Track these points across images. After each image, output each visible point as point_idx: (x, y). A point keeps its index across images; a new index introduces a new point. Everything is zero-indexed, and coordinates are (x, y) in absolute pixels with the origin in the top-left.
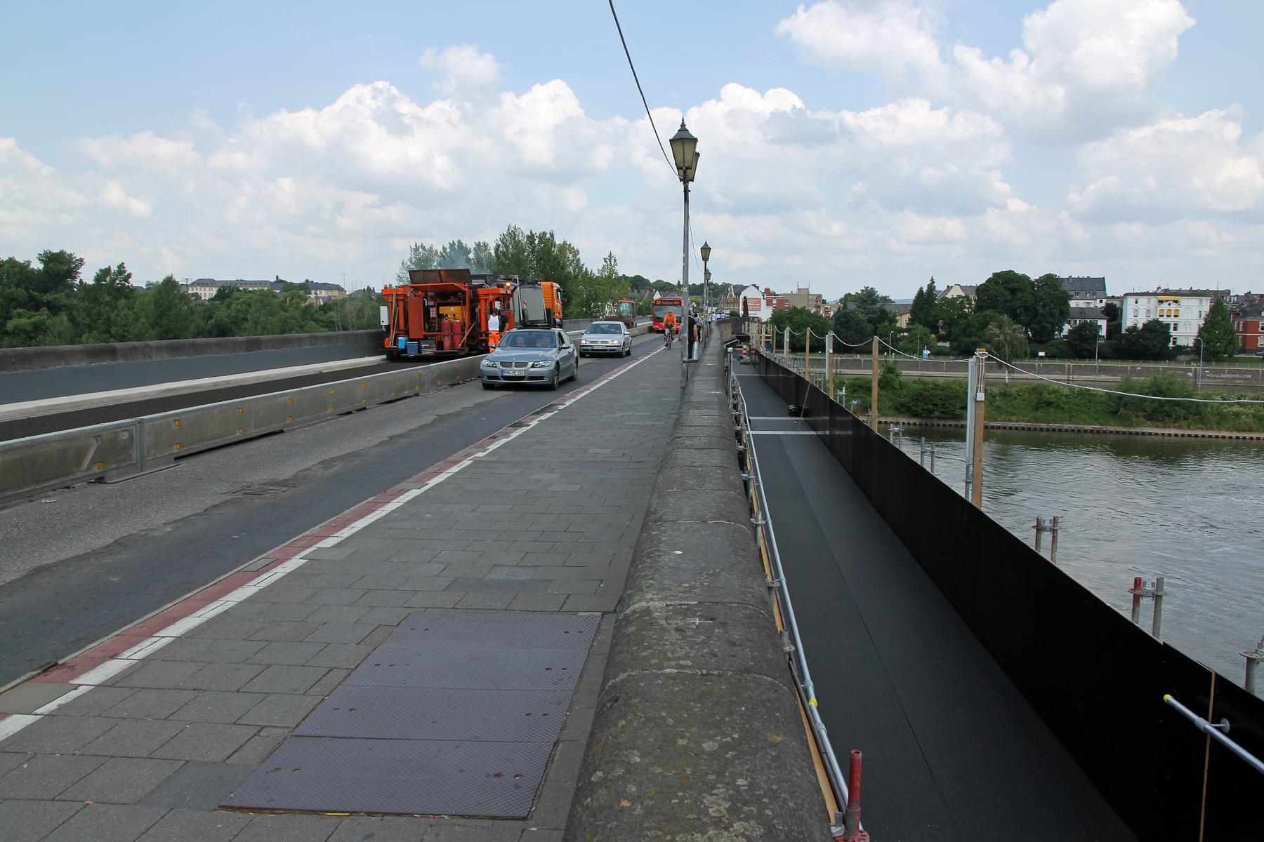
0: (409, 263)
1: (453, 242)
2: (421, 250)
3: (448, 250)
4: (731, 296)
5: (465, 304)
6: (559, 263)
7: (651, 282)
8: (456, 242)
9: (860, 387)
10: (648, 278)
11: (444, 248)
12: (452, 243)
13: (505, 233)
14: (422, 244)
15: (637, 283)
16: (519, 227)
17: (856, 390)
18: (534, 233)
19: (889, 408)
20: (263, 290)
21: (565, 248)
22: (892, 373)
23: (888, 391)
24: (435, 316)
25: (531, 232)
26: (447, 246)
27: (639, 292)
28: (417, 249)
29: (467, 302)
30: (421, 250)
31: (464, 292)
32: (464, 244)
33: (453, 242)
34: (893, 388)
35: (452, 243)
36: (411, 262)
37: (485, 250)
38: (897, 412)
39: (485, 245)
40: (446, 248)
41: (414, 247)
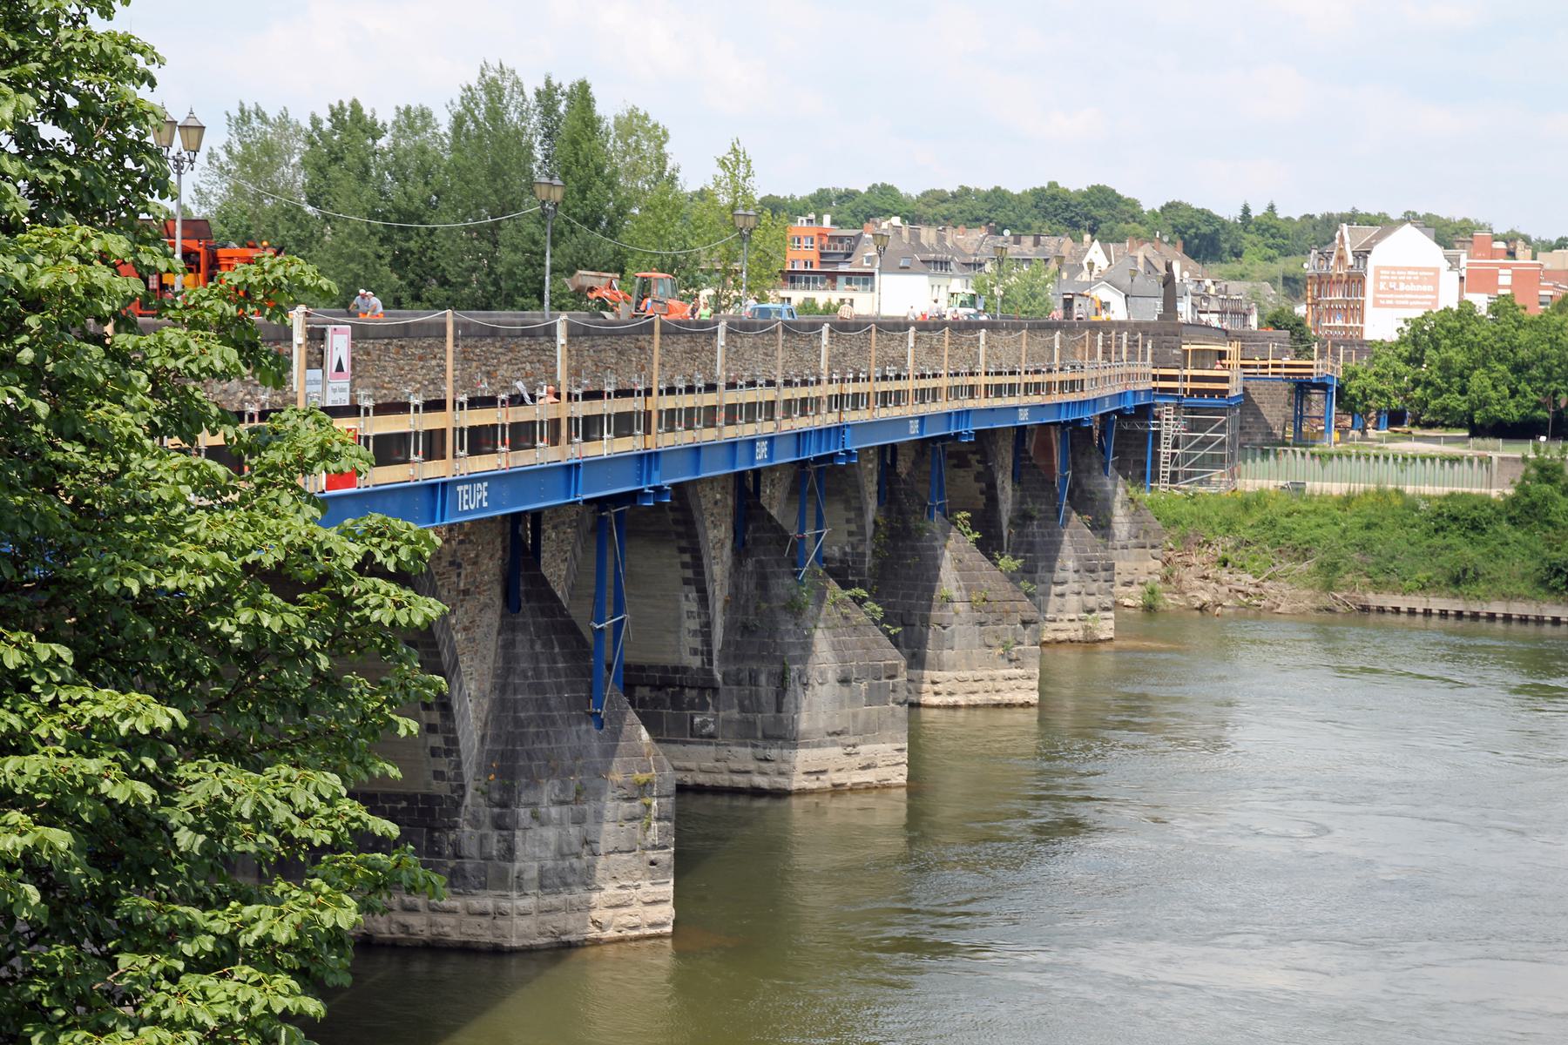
0: (224, 157)
1: (341, 103)
2: (255, 123)
3: (326, 126)
4: (1341, 259)
5: (199, 271)
6: (599, 171)
7: (1146, 207)
8: (346, 105)
9: (1455, 519)
10: (1132, 196)
11: (315, 122)
12: (336, 106)
13: (474, 84)
14: (258, 108)
15: (1095, 213)
16: (511, 67)
17: (1442, 529)
18: (555, 83)
19: (1524, 577)
20: (1488, 496)
21: (634, 125)
22: (1550, 481)
23: (1531, 532)
24: (155, 286)
25: (548, 83)
26: (324, 114)
27: (1037, 243)
28: (244, 118)
29: (202, 267)
30: (255, 123)
31: (198, 254)
32: (367, 112)
33: (341, 103)
34: (1550, 523)
35: (336, 106)
36: (229, 152)
37: (424, 129)
38: (1542, 590)
39: (425, 115)
40: (321, 122)
41: (236, 113)
